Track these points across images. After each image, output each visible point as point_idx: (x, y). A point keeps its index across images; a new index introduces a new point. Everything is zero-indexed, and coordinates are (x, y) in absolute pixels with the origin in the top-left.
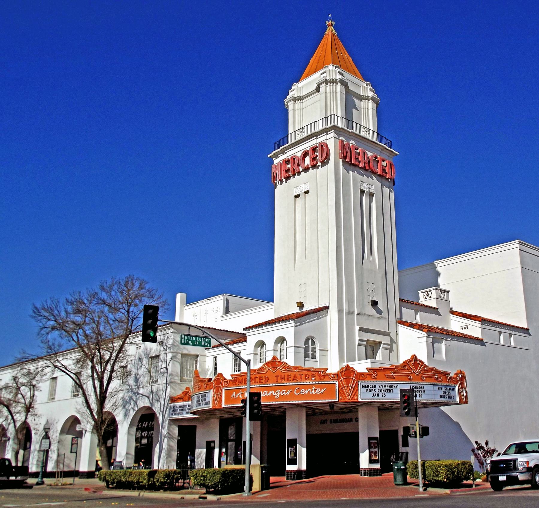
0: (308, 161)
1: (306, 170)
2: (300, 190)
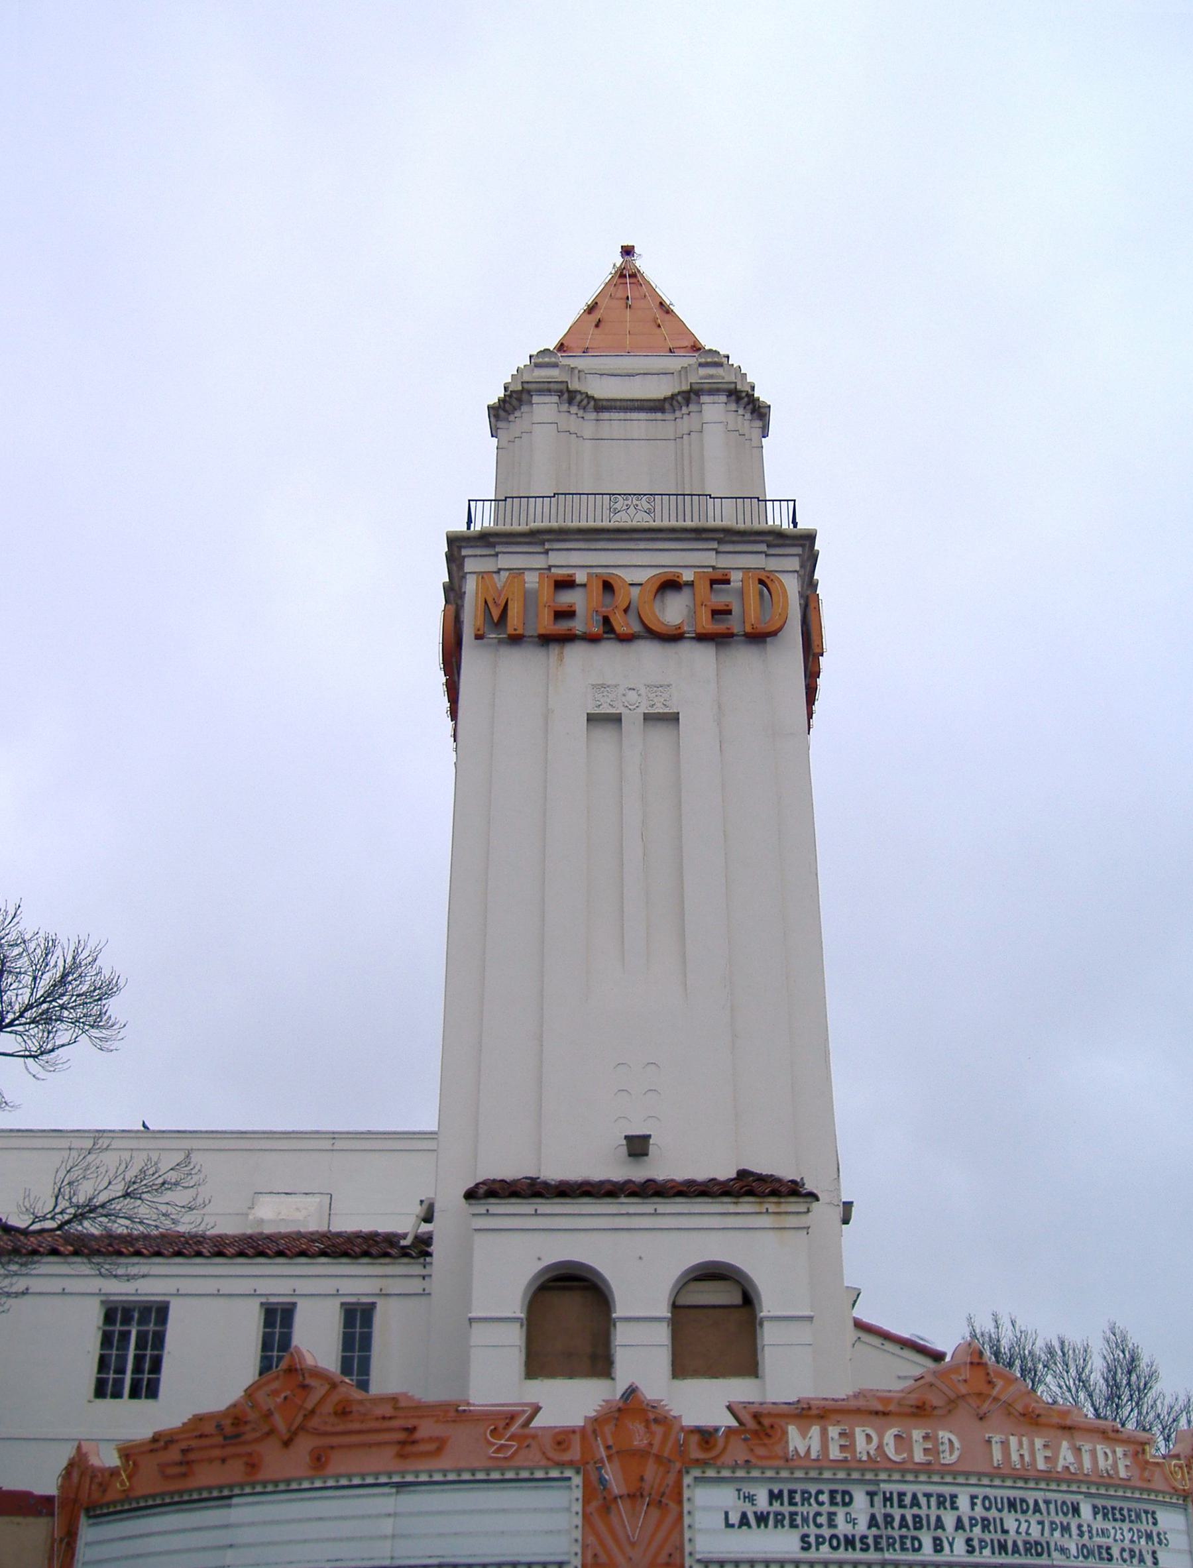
0: (674, 611)
1: (673, 637)
2: (634, 705)
